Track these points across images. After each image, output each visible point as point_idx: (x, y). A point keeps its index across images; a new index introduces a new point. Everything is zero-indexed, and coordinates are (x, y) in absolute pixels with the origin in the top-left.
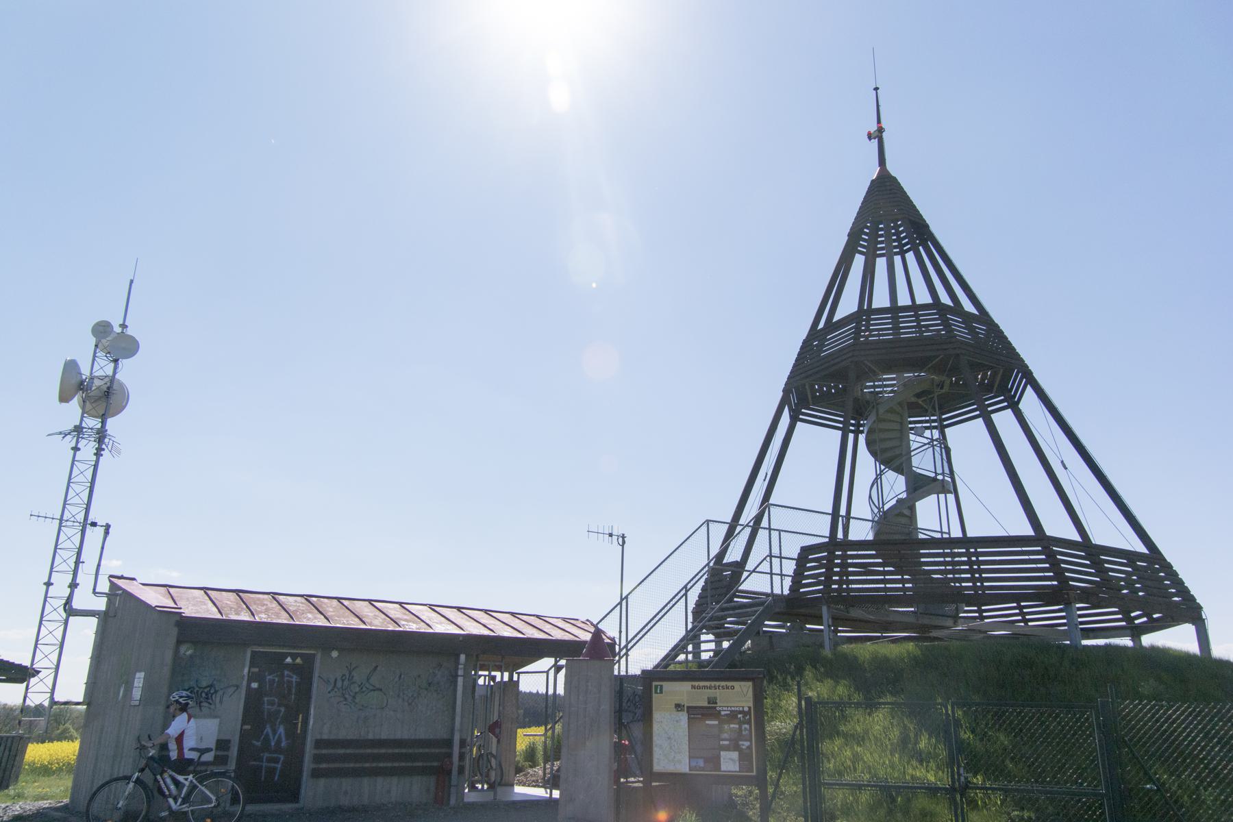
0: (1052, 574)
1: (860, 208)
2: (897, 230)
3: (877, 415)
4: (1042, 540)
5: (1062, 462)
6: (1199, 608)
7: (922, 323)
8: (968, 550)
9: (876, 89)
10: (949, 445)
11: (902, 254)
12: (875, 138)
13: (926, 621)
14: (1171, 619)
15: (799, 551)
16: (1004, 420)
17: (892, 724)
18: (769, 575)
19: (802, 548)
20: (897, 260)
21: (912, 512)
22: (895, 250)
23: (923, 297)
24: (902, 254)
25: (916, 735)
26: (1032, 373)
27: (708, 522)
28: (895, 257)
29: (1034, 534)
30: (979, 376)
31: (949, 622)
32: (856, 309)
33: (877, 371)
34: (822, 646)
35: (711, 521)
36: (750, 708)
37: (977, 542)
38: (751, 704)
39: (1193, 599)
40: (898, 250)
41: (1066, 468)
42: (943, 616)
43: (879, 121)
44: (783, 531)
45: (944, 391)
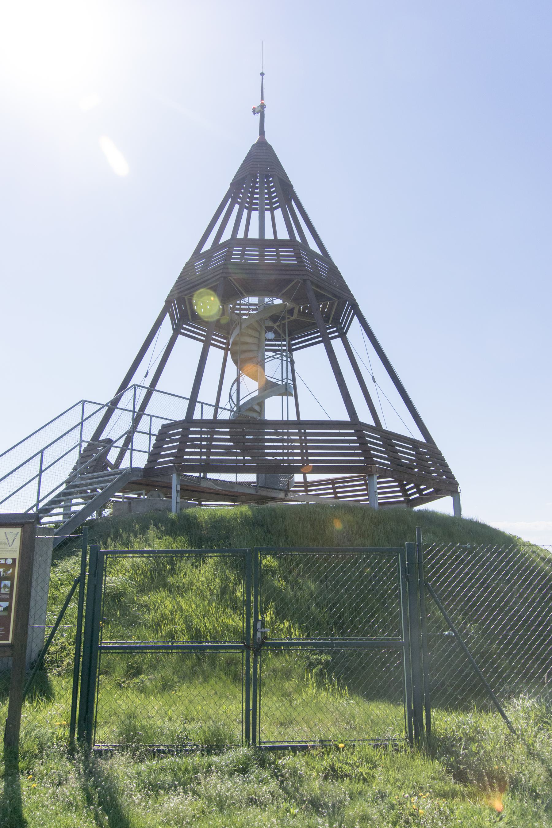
0: (360, 451)
1: (242, 165)
2: (268, 186)
3: (241, 329)
4: (357, 425)
5: (373, 377)
6: (457, 484)
7: (280, 254)
8: (300, 430)
9: (262, 74)
10: (294, 359)
11: (272, 210)
12: (258, 113)
13: (264, 493)
14: (438, 494)
15: (160, 428)
16: (337, 344)
17: (215, 575)
18: (133, 448)
19: (163, 425)
20: (268, 214)
21: (261, 409)
22: (266, 202)
23: (283, 235)
24: (272, 210)
25: (235, 584)
26: (358, 306)
27: (83, 402)
28: (266, 212)
29: (349, 420)
30: (321, 306)
31: (282, 495)
32: (230, 238)
33: (243, 292)
34: (170, 510)
35: (86, 401)
36: (14, 560)
37: (307, 424)
38: (17, 556)
39: (453, 478)
40: (269, 207)
41: (375, 382)
42: (276, 489)
43: (262, 99)
44: (153, 416)
45: (293, 318)
